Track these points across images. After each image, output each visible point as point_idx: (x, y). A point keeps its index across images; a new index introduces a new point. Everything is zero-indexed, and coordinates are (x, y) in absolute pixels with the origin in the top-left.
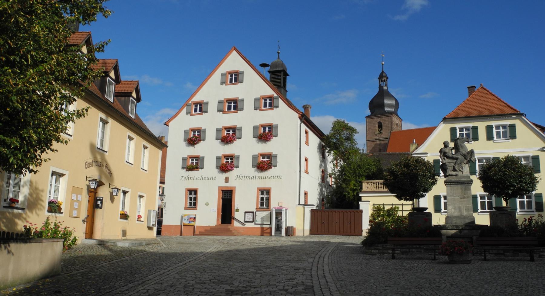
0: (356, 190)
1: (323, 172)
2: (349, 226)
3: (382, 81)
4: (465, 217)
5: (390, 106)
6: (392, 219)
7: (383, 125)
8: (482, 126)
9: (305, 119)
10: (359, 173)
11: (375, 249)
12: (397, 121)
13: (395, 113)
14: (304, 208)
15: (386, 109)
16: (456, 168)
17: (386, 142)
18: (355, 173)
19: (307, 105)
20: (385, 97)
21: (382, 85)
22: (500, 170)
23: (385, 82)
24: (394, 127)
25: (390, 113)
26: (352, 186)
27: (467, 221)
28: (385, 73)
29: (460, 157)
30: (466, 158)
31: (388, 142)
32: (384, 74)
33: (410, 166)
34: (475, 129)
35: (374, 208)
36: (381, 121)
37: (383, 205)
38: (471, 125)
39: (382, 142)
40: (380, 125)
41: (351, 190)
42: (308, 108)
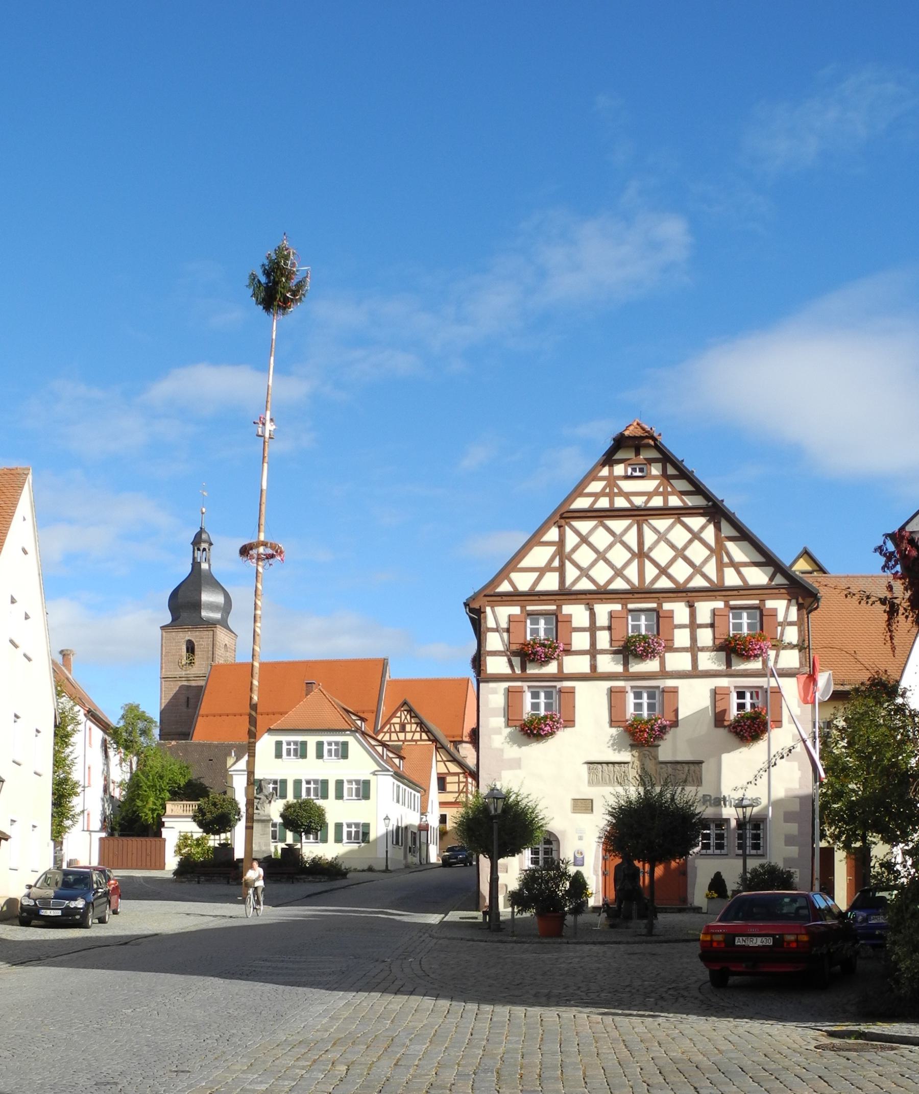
0: (155, 810)
1: (105, 779)
2: (148, 858)
3: (199, 549)
4: (264, 852)
5: (213, 607)
6: (202, 849)
7: (196, 647)
8: (312, 741)
9: (92, 716)
10: (160, 786)
11: (184, 878)
12: (226, 638)
13: (224, 623)
14: (90, 835)
15: (205, 614)
16: (259, 807)
17: (202, 683)
18: (154, 786)
19: (67, 650)
20: (203, 588)
21: (199, 561)
22: (295, 811)
23: (204, 552)
24: (220, 652)
25: (211, 625)
26: (151, 805)
27: (266, 855)
28: (206, 532)
29: (262, 797)
30: (267, 799)
31: (206, 684)
32: (204, 536)
33: (217, 805)
34: (304, 744)
35: (180, 836)
36: (193, 640)
37: (192, 832)
38: (300, 738)
39: (193, 684)
40: (191, 648)
41: (149, 810)
42: (68, 655)
